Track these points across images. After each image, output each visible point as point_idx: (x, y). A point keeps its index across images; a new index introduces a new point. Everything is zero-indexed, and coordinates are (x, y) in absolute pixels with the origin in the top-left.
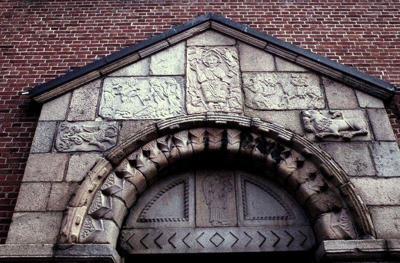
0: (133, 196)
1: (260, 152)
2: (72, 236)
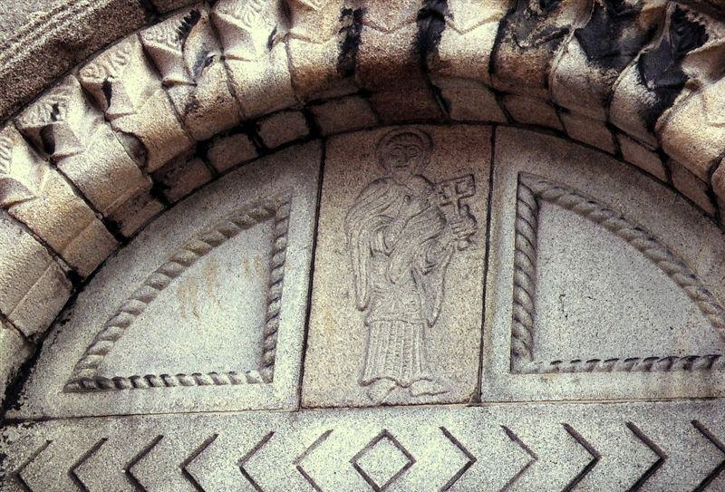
1: (582, 59)
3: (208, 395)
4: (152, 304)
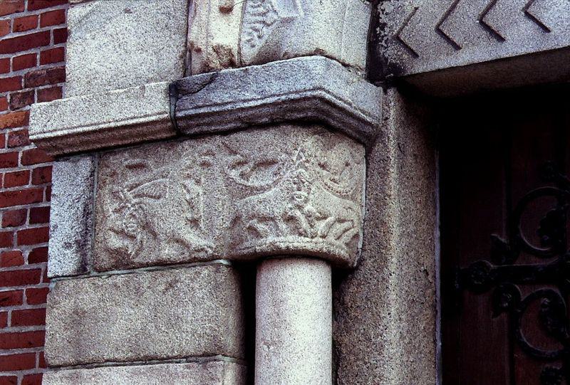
2: (217, 49)
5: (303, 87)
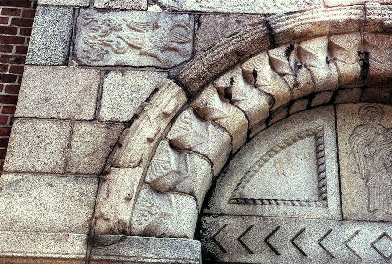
0: (224, 155)
3: (298, 211)
4: (262, 168)
5: (188, 257)
